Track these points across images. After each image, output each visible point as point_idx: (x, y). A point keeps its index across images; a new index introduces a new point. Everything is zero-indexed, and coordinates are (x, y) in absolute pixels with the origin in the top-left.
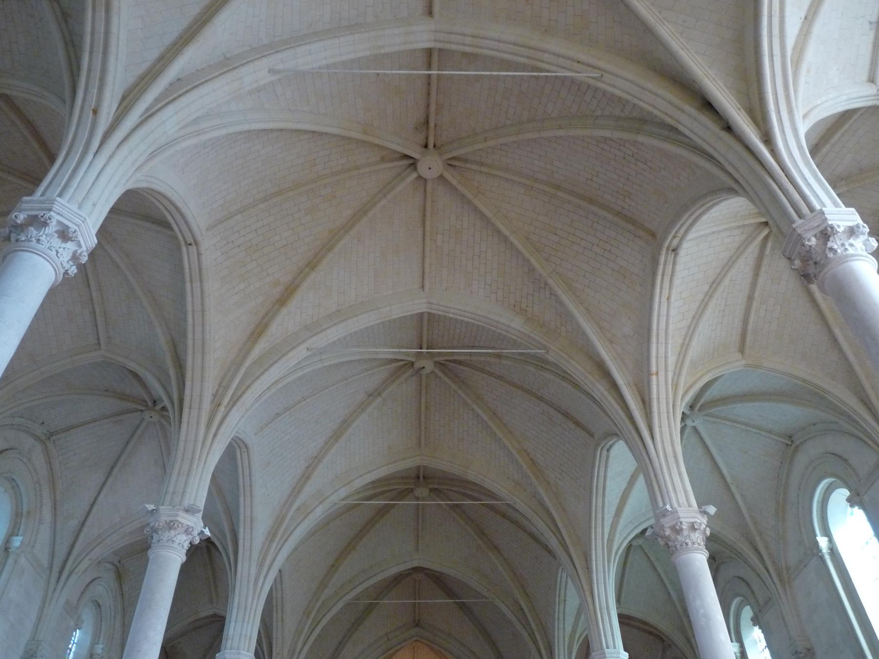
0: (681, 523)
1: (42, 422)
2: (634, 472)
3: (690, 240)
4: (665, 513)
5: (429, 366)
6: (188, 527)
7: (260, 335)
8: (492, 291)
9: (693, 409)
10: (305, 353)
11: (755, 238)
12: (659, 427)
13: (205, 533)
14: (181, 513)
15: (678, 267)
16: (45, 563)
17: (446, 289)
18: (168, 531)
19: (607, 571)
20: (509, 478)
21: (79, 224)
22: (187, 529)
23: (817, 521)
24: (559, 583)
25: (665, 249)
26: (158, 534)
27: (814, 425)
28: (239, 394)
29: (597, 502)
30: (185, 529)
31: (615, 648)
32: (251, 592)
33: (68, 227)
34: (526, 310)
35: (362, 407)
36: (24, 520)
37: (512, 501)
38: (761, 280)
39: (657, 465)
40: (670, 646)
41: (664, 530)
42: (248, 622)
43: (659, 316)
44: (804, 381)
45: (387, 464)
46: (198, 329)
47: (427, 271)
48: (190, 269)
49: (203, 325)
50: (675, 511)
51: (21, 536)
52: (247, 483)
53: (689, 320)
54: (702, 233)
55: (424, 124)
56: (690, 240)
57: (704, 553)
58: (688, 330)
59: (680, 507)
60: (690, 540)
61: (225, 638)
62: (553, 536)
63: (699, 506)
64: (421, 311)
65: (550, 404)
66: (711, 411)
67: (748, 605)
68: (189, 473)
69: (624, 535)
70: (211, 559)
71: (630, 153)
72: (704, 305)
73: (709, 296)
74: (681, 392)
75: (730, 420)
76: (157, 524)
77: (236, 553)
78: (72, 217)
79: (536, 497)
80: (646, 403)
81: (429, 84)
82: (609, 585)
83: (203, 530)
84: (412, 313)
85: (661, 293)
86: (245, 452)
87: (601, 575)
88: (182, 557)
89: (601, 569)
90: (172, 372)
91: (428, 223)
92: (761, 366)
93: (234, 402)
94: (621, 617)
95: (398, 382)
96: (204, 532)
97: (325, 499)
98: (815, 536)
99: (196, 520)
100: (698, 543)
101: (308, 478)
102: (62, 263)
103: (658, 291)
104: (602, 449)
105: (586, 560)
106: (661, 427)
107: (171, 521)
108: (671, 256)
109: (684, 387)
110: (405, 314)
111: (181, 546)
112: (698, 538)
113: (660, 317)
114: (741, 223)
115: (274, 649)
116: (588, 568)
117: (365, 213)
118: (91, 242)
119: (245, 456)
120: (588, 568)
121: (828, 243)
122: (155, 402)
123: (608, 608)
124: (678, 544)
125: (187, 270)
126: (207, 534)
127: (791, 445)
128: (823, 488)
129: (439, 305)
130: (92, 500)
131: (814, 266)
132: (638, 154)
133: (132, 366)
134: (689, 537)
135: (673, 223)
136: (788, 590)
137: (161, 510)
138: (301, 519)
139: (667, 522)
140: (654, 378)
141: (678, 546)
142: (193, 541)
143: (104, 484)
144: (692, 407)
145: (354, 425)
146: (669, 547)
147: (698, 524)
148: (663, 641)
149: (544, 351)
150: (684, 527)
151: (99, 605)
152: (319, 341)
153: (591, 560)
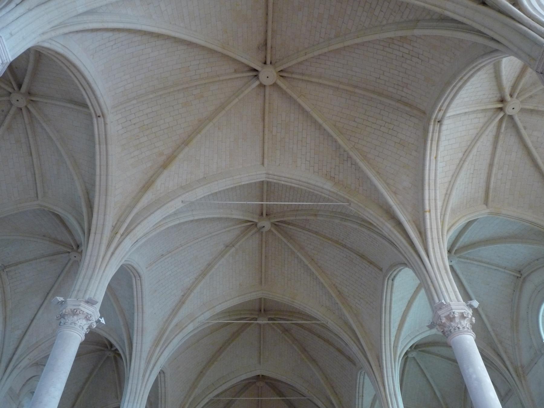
0: (454, 313)
2: (411, 299)
4: (441, 306)
5: (266, 224)
8: (310, 165)
9: (450, 253)
11: (494, 120)
12: (432, 249)
13: (101, 321)
14: (83, 304)
15: (443, 138)
17: (279, 165)
18: (72, 317)
19: (394, 367)
22: (87, 316)
24: (358, 384)
25: (433, 121)
26: (65, 319)
27: (538, 260)
28: (132, 227)
29: (385, 317)
30: (84, 316)
32: (140, 381)
34: (334, 178)
35: (222, 254)
37: (325, 321)
39: (432, 274)
42: (137, 403)
43: (429, 170)
44: (531, 223)
45: (238, 296)
46: (103, 178)
48: (99, 135)
49: (107, 175)
50: (448, 304)
52: (140, 303)
53: (450, 178)
55: (264, 45)
57: (471, 334)
60: (461, 325)
62: (355, 345)
64: (262, 180)
66: (462, 254)
68: (91, 277)
70: (117, 366)
71: (407, 51)
72: (460, 167)
73: (463, 161)
74: (446, 228)
75: (476, 261)
77: (131, 354)
80: (422, 234)
81: (267, 14)
83: (100, 319)
84: (256, 181)
85: (431, 153)
86: (138, 280)
87: (389, 370)
88: (81, 336)
89: (389, 365)
90: (84, 210)
91: (266, 117)
92: (501, 214)
93: (128, 231)
95: (246, 237)
99: (94, 310)
100: (467, 328)
101: (183, 303)
104: (388, 279)
105: (379, 361)
106: (434, 248)
107: (74, 309)
108: (437, 126)
111: (81, 327)
112: (466, 323)
114: (484, 107)
116: (380, 366)
120: (380, 366)
123: (395, 395)
126: (103, 322)
127: (520, 277)
129: (274, 175)
130: (33, 316)
132: (413, 51)
133: (59, 211)
135: (439, 98)
136: (523, 382)
137: (67, 302)
138: (178, 332)
139: (443, 313)
140: (427, 214)
141: (452, 330)
142: (92, 326)
143: (41, 305)
145: (216, 267)
147: (467, 314)
149: (348, 204)
150: (456, 316)
153: (382, 360)
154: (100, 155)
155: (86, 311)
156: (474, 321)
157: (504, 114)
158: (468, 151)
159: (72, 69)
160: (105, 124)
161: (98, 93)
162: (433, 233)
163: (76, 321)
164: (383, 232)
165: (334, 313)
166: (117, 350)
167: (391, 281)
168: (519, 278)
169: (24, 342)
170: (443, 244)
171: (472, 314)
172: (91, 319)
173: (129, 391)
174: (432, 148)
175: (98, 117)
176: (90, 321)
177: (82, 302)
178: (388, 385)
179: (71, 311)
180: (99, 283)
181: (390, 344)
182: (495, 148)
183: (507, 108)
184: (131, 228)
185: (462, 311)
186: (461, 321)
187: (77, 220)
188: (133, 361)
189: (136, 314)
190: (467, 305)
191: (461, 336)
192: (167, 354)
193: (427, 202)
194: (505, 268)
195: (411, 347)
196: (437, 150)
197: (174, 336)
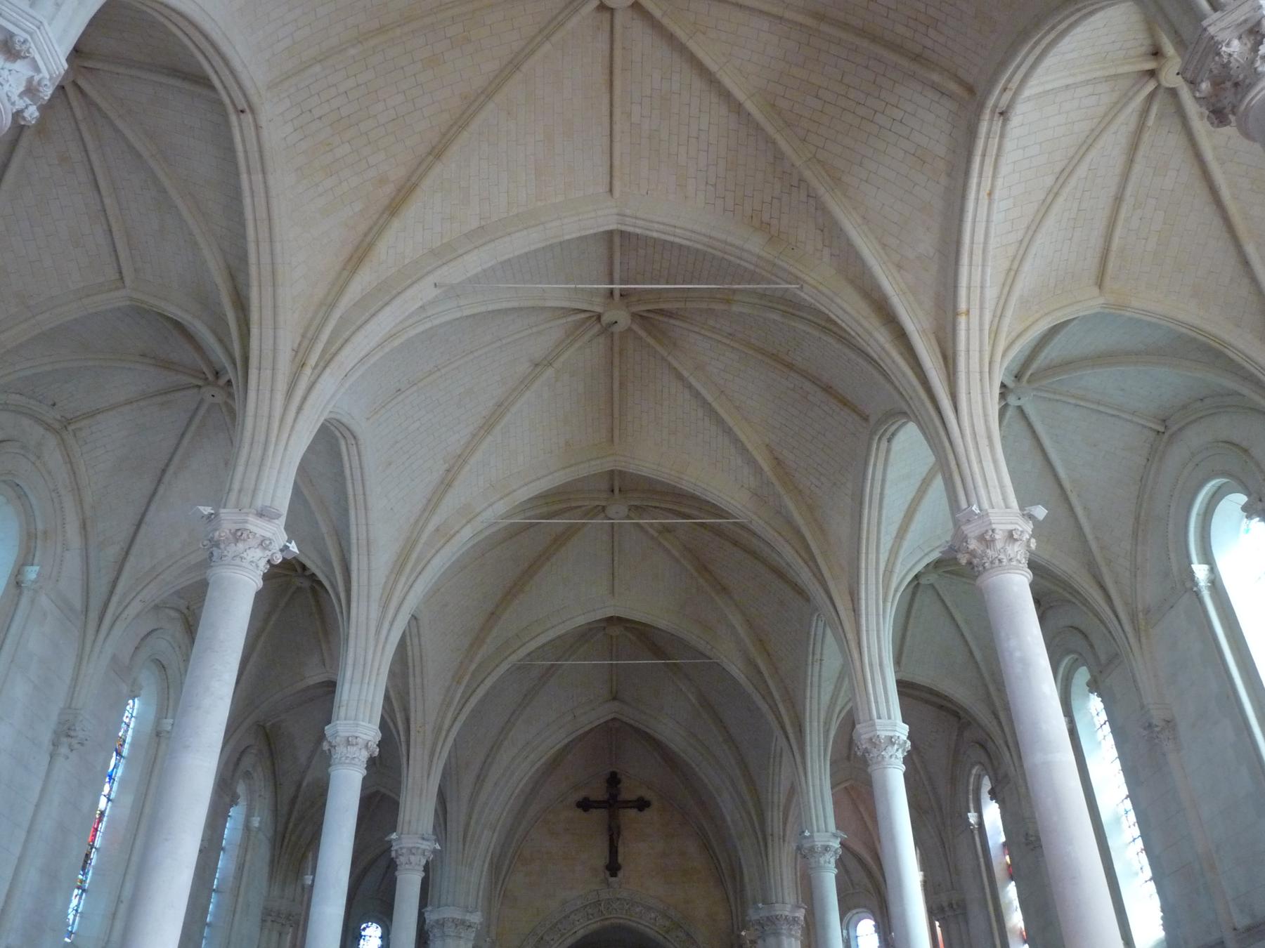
0: (993, 531)
1: (52, 402)
2: (927, 475)
3: (1029, 99)
6: (264, 539)
7: (361, 260)
9: (1019, 380)
10: (432, 293)
11: (1136, 94)
12: (966, 394)
13: (291, 548)
14: (251, 519)
15: (1009, 145)
16: (78, 604)
17: (647, 193)
18: (233, 545)
20: (742, 486)
21: (33, 31)
22: (262, 542)
23: (1195, 541)
28: (333, 349)
30: (259, 541)
31: (889, 718)
33: (12, 35)
36: (39, 543)
38: (1138, 168)
40: (969, 724)
41: (966, 542)
43: (974, 222)
46: (265, 246)
47: (617, 163)
51: (38, 565)
54: (1049, 87)
56: (1029, 99)
57: (1025, 573)
58: (1019, 247)
59: (993, 508)
61: (338, 705)
62: (806, 569)
63: (1022, 508)
65: (804, 374)
67: (1083, 665)
69: (909, 566)
72: (1046, 208)
73: (1053, 194)
76: (217, 533)
78: (20, 18)
83: (288, 544)
85: (979, 184)
88: (257, 581)
89: (873, 609)
92: (1129, 307)
93: (326, 361)
94: (900, 683)
95: (577, 345)
96: (289, 547)
97: (475, 517)
98: (1190, 563)
99: (275, 529)
100: (1017, 560)
101: (449, 485)
102: (9, 94)
103: (974, 181)
106: (970, 393)
109: (1007, 337)
110: (584, 233)
112: (1018, 552)
113: (976, 224)
114: (1112, 71)
115: (412, 726)
117: (517, 68)
118: (55, 64)
119: (354, 450)
120: (854, 611)
121: (1261, 47)
122: (217, 373)
123: (881, 665)
124: (988, 561)
125: (241, 155)
127: (1164, 433)
128: (1207, 494)
129: (636, 218)
131: (1233, 90)
134: (1004, 551)
135: (1003, 64)
136: (1143, 640)
138: (442, 542)
139: (972, 530)
140: (962, 320)
141: (987, 564)
144: (1018, 377)
146: (973, 568)
147: (1019, 533)
148: (960, 718)
149: (798, 286)
150: (997, 537)
151: (163, 667)
152: (454, 273)
153: (859, 599)
154: (253, 197)
157: (1156, 85)
158: (1068, 170)
159: (175, 17)
160: (257, 127)
161: (236, 63)
162: (971, 361)
163: (243, 553)
167: (886, 443)
168: (1160, 434)
170: (990, 383)
171: (1032, 531)
173: (350, 661)
174: (984, 174)
175: (241, 113)
178: (869, 648)
180: (279, 472)
182: (1131, 161)
183: (1164, 74)
184: (332, 350)
185: (1010, 527)
187: (214, 332)
188: (354, 605)
189: (352, 513)
190: (1023, 515)
192: (420, 588)
193: (963, 292)
194: (1134, 413)
196: (994, 177)
197: (433, 551)
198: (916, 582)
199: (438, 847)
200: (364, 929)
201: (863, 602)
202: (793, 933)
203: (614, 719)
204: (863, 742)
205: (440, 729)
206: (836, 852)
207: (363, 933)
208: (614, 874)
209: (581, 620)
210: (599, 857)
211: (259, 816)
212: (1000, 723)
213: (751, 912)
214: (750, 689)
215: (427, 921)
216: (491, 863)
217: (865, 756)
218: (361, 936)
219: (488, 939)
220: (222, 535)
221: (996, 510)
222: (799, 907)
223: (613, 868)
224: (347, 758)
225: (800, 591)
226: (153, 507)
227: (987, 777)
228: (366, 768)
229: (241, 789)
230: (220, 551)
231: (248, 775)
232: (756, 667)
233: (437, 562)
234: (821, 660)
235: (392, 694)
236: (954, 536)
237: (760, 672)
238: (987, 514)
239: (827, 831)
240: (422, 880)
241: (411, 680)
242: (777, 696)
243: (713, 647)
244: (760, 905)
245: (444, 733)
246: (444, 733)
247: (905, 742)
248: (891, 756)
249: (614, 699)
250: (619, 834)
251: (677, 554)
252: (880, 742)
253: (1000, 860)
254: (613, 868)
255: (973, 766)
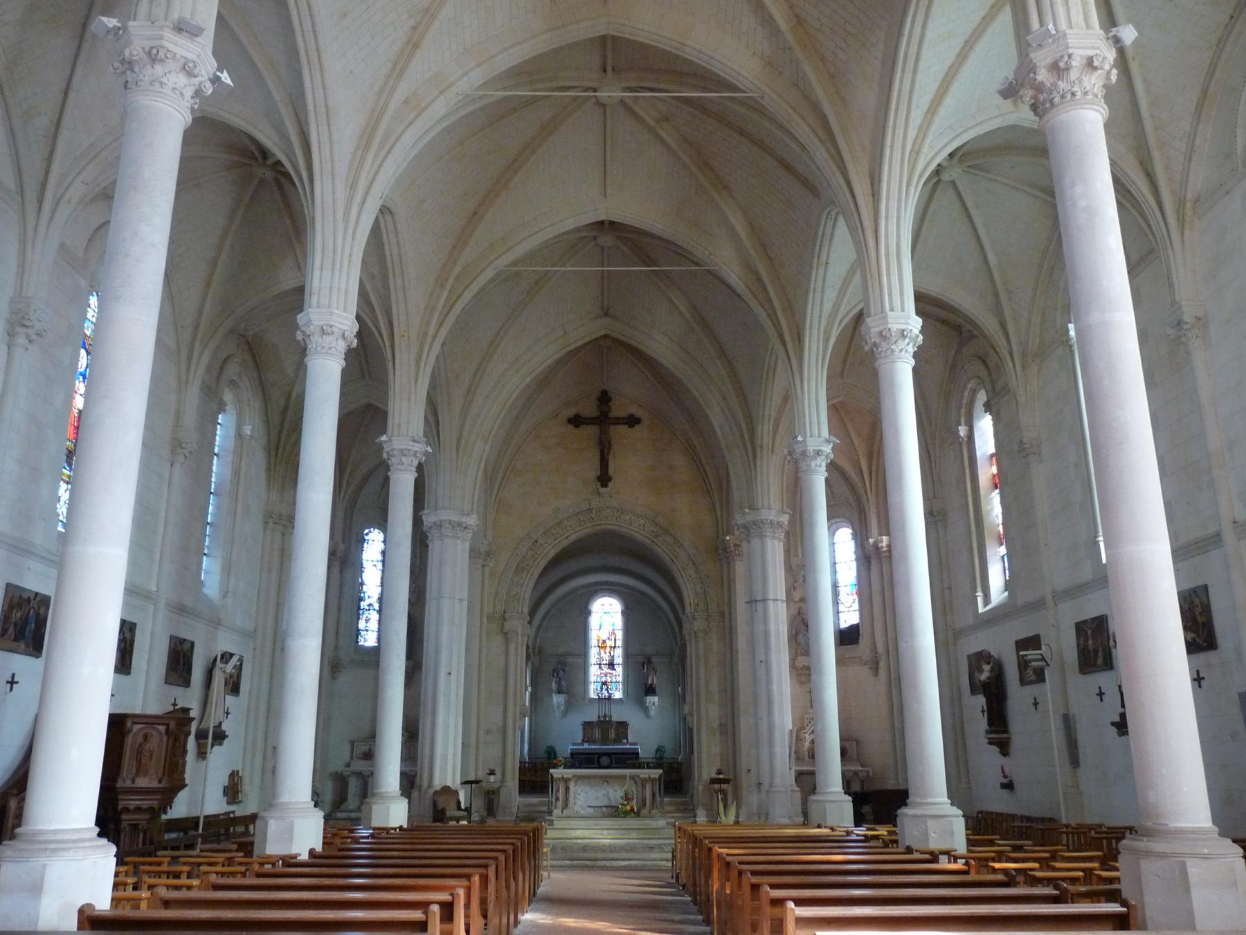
0: (1070, 56)
13: (223, 79)
14: (168, 34)
18: (149, 67)
22: (185, 64)
30: (181, 64)
31: (903, 310)
41: (1035, 74)
57: (1100, 108)
69: (937, 149)
79: (797, 85)
82: (905, 222)
83: (218, 73)
87: (894, 204)
99: (199, 50)
101: (416, 46)
105: (872, 185)
107: (152, 48)
111: (178, 92)
112: (1094, 83)
115: (396, 330)
120: (873, 196)
123: (898, 255)
134: (1080, 82)
136: (1187, 233)
138: (412, 116)
141: (1056, 99)
147: (1101, 59)
150: (1074, 63)
153: (880, 182)
155: (180, 52)
156: (1114, 78)
164: (869, 509)
165: (780, 73)
166: (279, 163)
169: (60, 148)
171: (1114, 61)
172: (196, 71)
176: (196, 77)
177: (165, 29)
178: (886, 236)
179: (145, 52)
181: (904, 147)
185: (1090, 53)
186: (1083, 78)
189: (306, 73)
191: (1074, 112)
192: (392, 169)
195: (951, 155)
197: (403, 127)
198: (935, 180)
199: (429, 449)
200: (367, 534)
201: (884, 186)
202: (777, 535)
203: (606, 336)
204: (872, 336)
205: (425, 334)
206: (827, 457)
207: (366, 537)
208: (604, 485)
209: (570, 224)
210: (593, 472)
211: (249, 424)
212: (1007, 335)
213: (737, 516)
214: (747, 296)
215: (425, 523)
216: (485, 471)
217: (873, 351)
218: (364, 540)
219: (485, 542)
220: (135, 53)
221: (1075, 31)
222: (783, 512)
223: (604, 479)
224: (323, 347)
225: (812, 188)
226: (79, 71)
227: (983, 392)
228: (345, 359)
229: (228, 396)
230: (134, 75)
231: (233, 384)
232: (756, 274)
233: (408, 138)
234: (827, 263)
235: (368, 287)
236: (1018, 70)
237: (760, 280)
238: (1065, 35)
239: (819, 436)
240: (416, 480)
241: (391, 281)
242: (776, 304)
243: (711, 254)
244: (747, 510)
245: (429, 339)
246: (429, 339)
247: (917, 336)
248: (901, 350)
249: (606, 315)
250: (609, 448)
251: (674, 146)
252: (891, 335)
253: (987, 472)
254: (604, 479)
255: (969, 381)
